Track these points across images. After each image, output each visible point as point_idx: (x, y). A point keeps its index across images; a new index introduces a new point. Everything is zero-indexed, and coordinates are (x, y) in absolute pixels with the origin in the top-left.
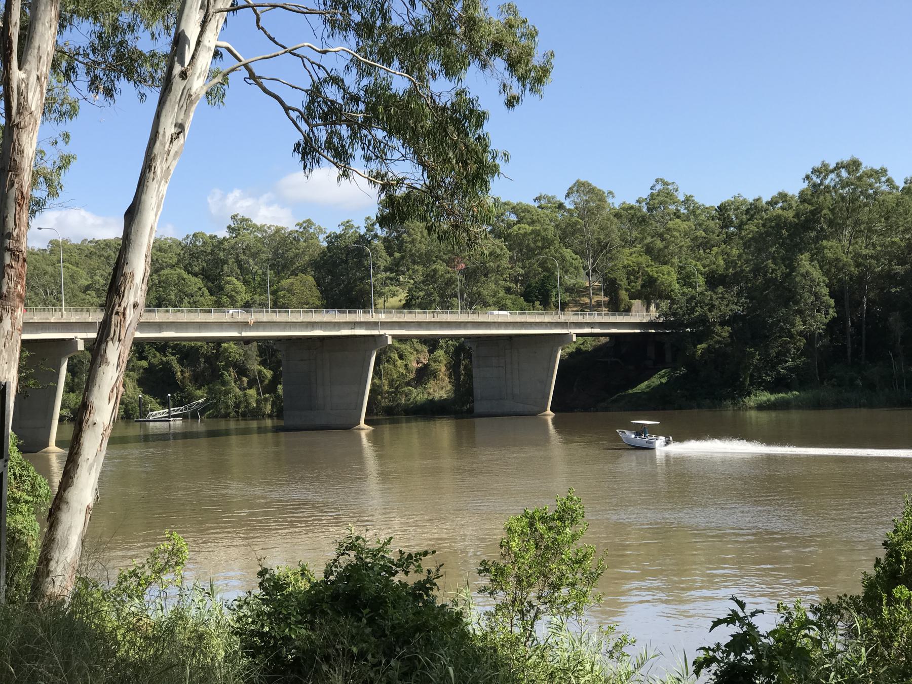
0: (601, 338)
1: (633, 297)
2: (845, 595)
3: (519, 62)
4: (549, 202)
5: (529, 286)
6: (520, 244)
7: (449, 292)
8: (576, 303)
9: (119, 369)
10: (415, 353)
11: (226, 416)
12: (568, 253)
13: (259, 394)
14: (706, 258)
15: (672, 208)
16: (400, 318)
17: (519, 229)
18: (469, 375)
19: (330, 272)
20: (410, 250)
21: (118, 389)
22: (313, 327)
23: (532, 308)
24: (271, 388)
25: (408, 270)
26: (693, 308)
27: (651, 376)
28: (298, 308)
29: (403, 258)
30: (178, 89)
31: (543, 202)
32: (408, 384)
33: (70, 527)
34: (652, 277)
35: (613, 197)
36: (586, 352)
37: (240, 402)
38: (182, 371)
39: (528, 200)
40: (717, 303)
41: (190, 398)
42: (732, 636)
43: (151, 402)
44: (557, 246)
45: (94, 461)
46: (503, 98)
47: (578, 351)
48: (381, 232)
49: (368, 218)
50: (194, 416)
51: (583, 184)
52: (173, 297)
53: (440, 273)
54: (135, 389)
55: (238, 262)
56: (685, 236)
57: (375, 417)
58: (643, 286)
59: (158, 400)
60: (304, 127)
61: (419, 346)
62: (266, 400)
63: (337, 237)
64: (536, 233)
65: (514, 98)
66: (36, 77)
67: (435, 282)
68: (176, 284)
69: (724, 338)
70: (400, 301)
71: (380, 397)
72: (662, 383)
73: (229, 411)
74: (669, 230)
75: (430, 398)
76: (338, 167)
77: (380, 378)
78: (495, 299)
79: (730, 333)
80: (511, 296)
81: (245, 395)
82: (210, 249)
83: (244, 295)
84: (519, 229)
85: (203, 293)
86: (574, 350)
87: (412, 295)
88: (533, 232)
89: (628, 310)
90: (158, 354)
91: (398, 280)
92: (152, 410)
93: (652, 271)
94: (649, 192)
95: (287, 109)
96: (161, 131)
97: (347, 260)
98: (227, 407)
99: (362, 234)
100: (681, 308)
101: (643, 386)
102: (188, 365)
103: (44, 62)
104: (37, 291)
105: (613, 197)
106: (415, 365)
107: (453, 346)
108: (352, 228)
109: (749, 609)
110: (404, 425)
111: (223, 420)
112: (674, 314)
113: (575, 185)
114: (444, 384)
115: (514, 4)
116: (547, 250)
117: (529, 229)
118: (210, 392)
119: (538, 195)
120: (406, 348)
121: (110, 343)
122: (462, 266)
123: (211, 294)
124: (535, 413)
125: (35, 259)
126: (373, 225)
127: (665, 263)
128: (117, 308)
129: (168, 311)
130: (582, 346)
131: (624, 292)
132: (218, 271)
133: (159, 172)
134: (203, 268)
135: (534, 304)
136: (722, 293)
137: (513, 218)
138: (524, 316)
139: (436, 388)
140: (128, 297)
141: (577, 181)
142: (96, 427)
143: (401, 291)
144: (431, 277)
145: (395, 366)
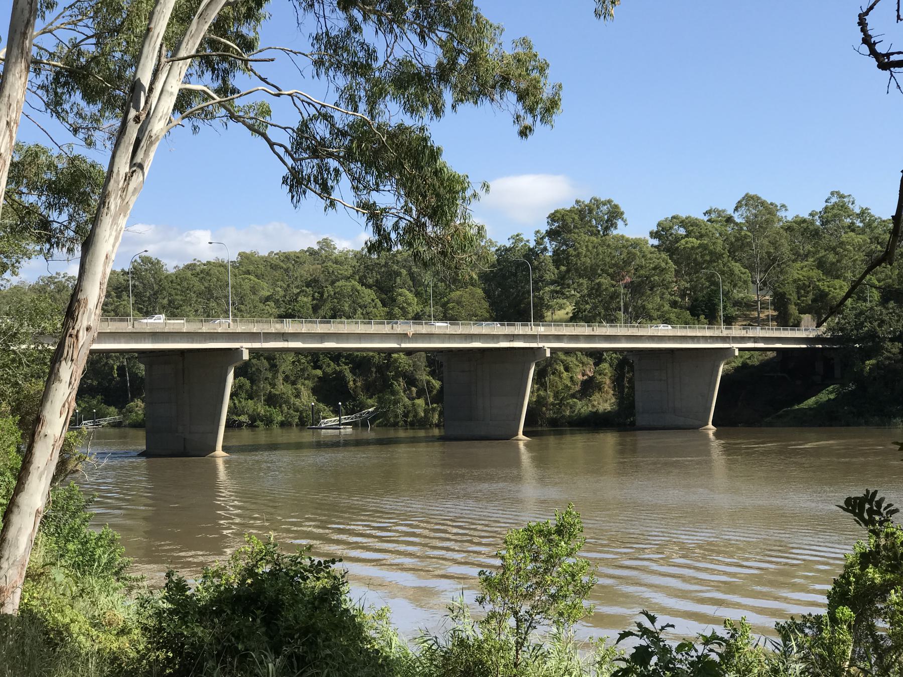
0: (769, 353)
1: (802, 311)
2: (810, 615)
3: (528, 94)
4: (719, 216)
5: (696, 300)
6: (688, 258)
7: (614, 305)
8: (746, 317)
9: (71, 386)
10: (581, 365)
11: (395, 425)
12: (737, 267)
13: (427, 404)
14: (881, 272)
15: (848, 221)
16: (559, 330)
17: (687, 243)
18: (632, 388)
19: (499, 285)
20: (576, 264)
21: (69, 405)
22: (472, 339)
23: (696, 322)
24: (439, 398)
25: (573, 283)
26: (862, 323)
27: (819, 391)
28: (467, 320)
29: (568, 271)
30: (131, 132)
31: (713, 216)
32: (573, 396)
33: (20, 529)
34: (823, 291)
35: (786, 210)
36: (753, 366)
37: (409, 412)
38: (354, 381)
39: (698, 214)
40: (887, 318)
41: (363, 406)
42: (635, 648)
43: (325, 410)
44: (725, 260)
45: (45, 469)
46: (517, 128)
47: (745, 365)
48: (550, 246)
49: (538, 232)
50: (364, 425)
51: (752, 198)
52: (347, 309)
53: (604, 287)
54: (309, 397)
55: (411, 275)
56: (859, 249)
57: (540, 429)
58: (814, 301)
59: (331, 408)
60: (290, 162)
61: (585, 359)
62: (434, 410)
63: (507, 250)
64: (704, 247)
65: (526, 128)
66: (5, 122)
67: (600, 296)
68: (351, 296)
69: (894, 354)
70: (567, 313)
71: (544, 409)
72: (830, 399)
73: (399, 420)
74: (842, 243)
75: (595, 410)
76: (322, 198)
77: (546, 390)
78: (659, 313)
79: (900, 349)
80: (676, 310)
81: (413, 405)
82: (383, 261)
83: (415, 307)
84: (686, 243)
85: (375, 305)
86: (740, 365)
87: (579, 308)
88: (700, 246)
89: (797, 325)
90: (332, 364)
91: (563, 294)
92: (324, 418)
93: (823, 286)
94: (824, 205)
95: (272, 145)
96: (115, 170)
97: (516, 273)
98: (396, 416)
99: (531, 247)
100: (849, 323)
101: (811, 401)
102: (361, 375)
103: (14, 109)
104: (219, 301)
105: (786, 210)
106: (580, 377)
107: (617, 358)
108: (522, 241)
109: (658, 625)
110: (568, 435)
111: (393, 428)
112: (842, 330)
113: (743, 198)
114: (609, 397)
115: (529, 38)
116: (715, 264)
117: (696, 242)
118: (380, 401)
119: (708, 208)
120: (571, 360)
121: (63, 363)
122: (628, 279)
123: (384, 305)
124: (697, 426)
125: (218, 271)
126: (542, 238)
127: (838, 277)
128: (70, 330)
129: (341, 323)
130: (748, 361)
131: (794, 307)
132: (391, 284)
133: (112, 207)
134: (377, 280)
135: (698, 318)
136: (893, 308)
137: (682, 231)
138: (685, 330)
139: (601, 401)
140: (81, 321)
141: (747, 195)
142: (47, 439)
143: (568, 304)
144: (596, 291)
145: (561, 378)
